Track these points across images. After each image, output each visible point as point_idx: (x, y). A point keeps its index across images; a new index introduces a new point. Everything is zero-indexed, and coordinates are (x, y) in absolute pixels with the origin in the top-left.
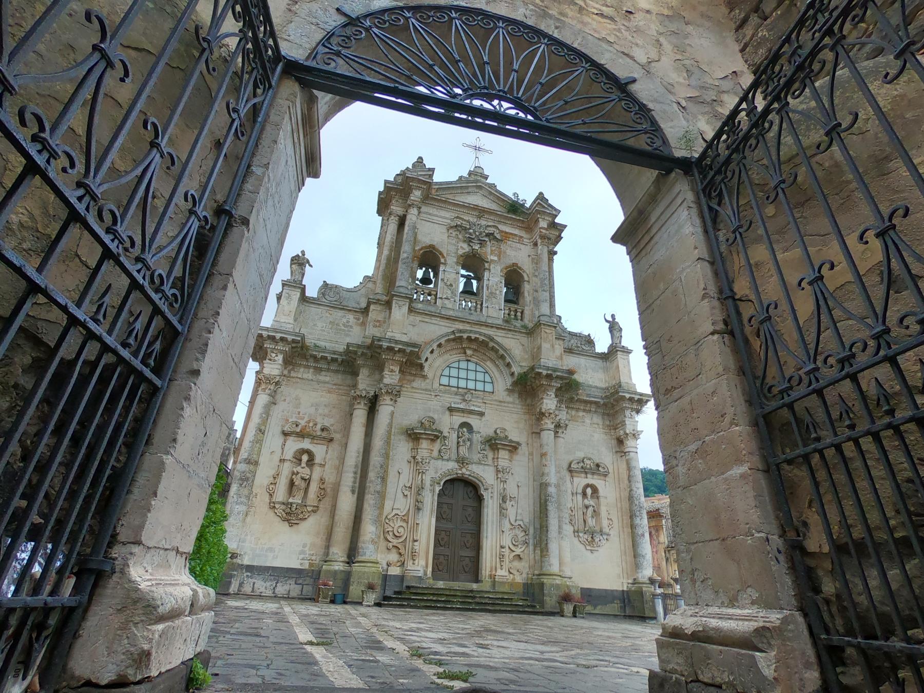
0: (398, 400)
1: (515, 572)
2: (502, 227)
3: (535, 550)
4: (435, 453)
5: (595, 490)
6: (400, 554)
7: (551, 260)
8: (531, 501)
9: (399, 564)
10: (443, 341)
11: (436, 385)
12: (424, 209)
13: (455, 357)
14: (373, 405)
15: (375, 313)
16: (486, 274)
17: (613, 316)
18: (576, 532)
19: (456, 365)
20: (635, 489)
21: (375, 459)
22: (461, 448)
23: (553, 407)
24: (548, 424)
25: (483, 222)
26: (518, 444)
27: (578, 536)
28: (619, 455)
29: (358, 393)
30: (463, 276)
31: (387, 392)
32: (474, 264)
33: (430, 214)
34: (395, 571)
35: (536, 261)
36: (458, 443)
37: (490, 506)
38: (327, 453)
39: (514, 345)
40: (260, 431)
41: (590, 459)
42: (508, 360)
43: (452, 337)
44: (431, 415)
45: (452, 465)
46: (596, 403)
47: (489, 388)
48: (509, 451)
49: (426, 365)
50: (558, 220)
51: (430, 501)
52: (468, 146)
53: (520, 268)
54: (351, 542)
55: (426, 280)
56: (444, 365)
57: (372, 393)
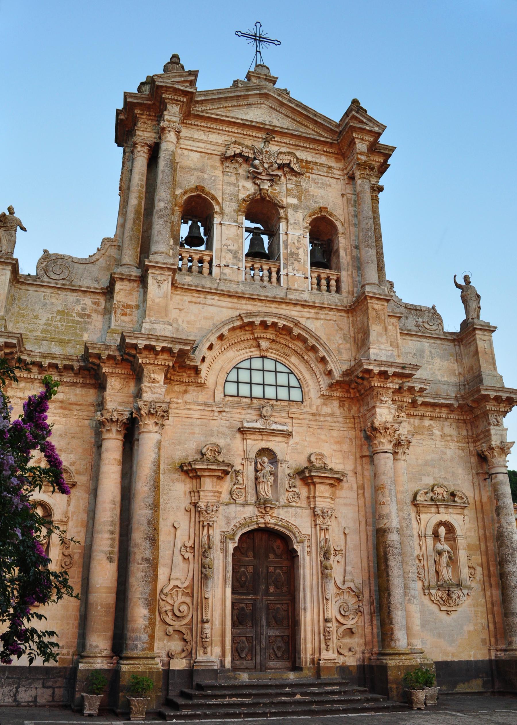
0: (166, 423)
1: (347, 653)
2: (301, 154)
3: (371, 621)
4: (225, 497)
5: (450, 528)
6: (185, 640)
7: (375, 200)
8: (364, 554)
10: (225, 330)
11: (219, 396)
12: (185, 132)
13: (245, 354)
14: (131, 431)
15: (123, 293)
16: (283, 225)
17: (466, 279)
18: (426, 589)
19: (246, 364)
20: (504, 524)
21: (141, 512)
22: (261, 486)
23: (389, 418)
24: (385, 443)
25: (273, 148)
26: (343, 474)
27: (430, 594)
28: (481, 477)
29: (107, 416)
30: (248, 230)
31: (150, 414)
32: (263, 213)
33: (194, 140)
34: (179, 664)
35: (356, 202)
36: (256, 478)
37: (307, 564)
38: (68, 504)
39: (326, 328)
41: (441, 486)
42: (322, 353)
43: (238, 323)
44: (214, 440)
45: (250, 511)
46: (447, 406)
47: (296, 395)
48: (331, 485)
49: (204, 368)
50: (383, 140)
51: (221, 564)
52: (244, 35)
53: (331, 215)
54: (116, 627)
55: (193, 240)
57: (127, 415)
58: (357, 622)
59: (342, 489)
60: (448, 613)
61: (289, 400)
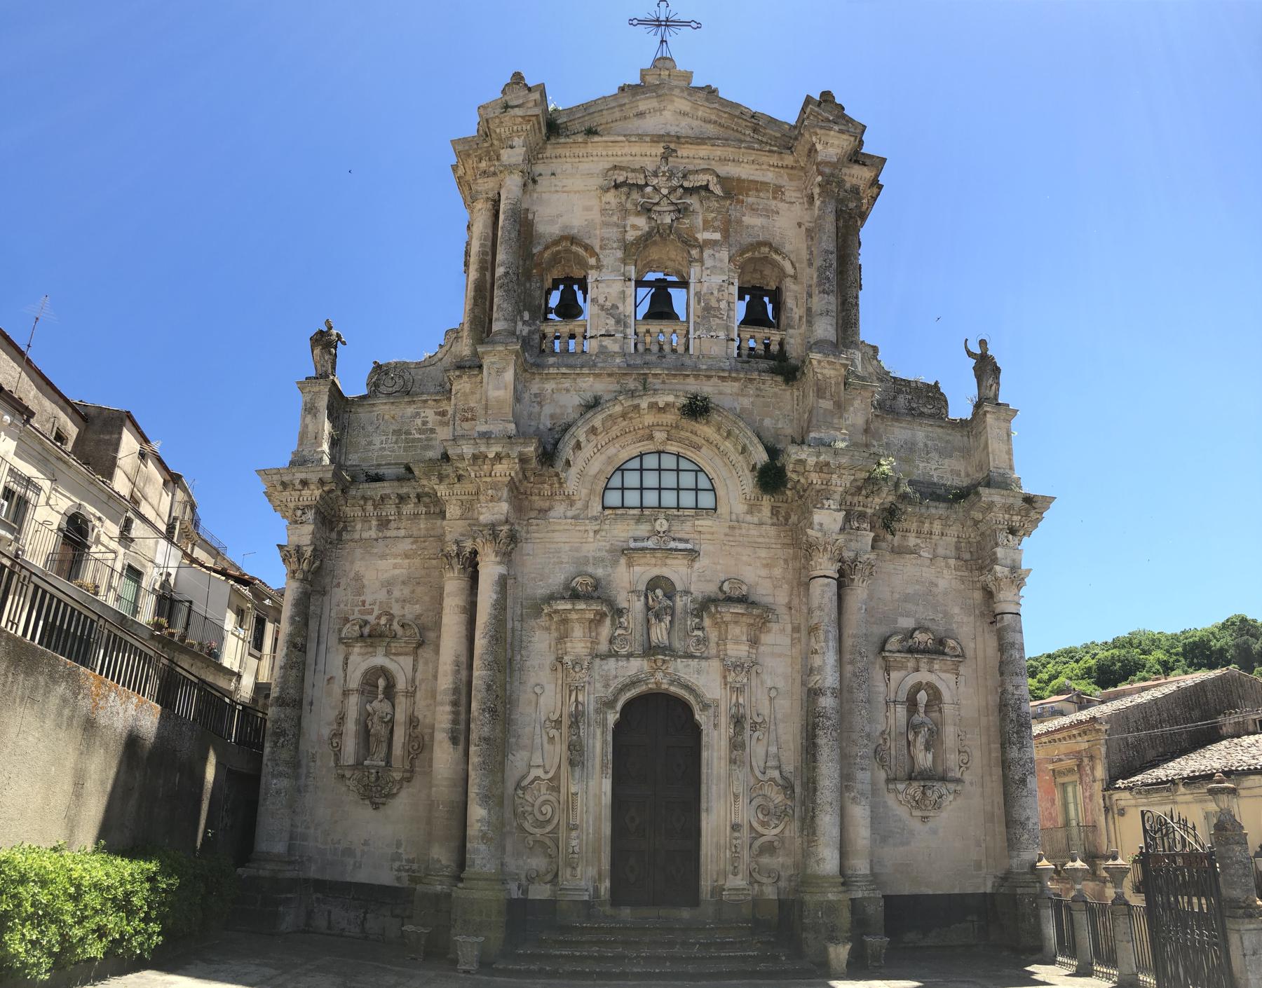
9: (549, 878)
34: (540, 892)
40: (295, 646)
51: (599, 744)
56: (611, 469)
58: (782, 831)
59: (769, 631)
60: (924, 819)
61: (697, 508)
